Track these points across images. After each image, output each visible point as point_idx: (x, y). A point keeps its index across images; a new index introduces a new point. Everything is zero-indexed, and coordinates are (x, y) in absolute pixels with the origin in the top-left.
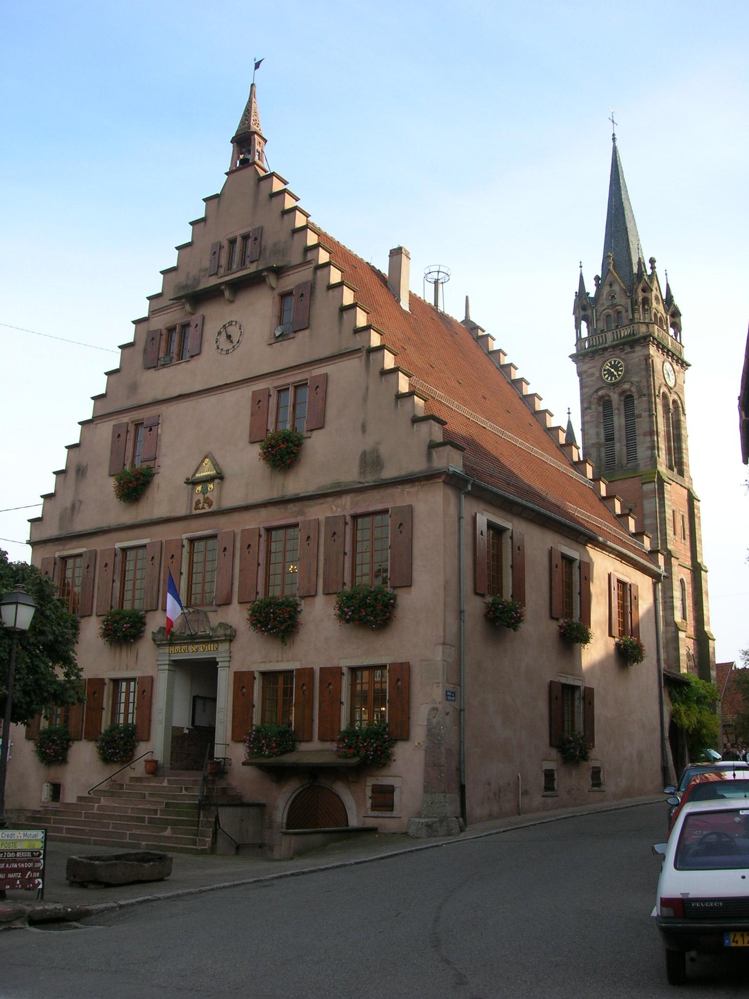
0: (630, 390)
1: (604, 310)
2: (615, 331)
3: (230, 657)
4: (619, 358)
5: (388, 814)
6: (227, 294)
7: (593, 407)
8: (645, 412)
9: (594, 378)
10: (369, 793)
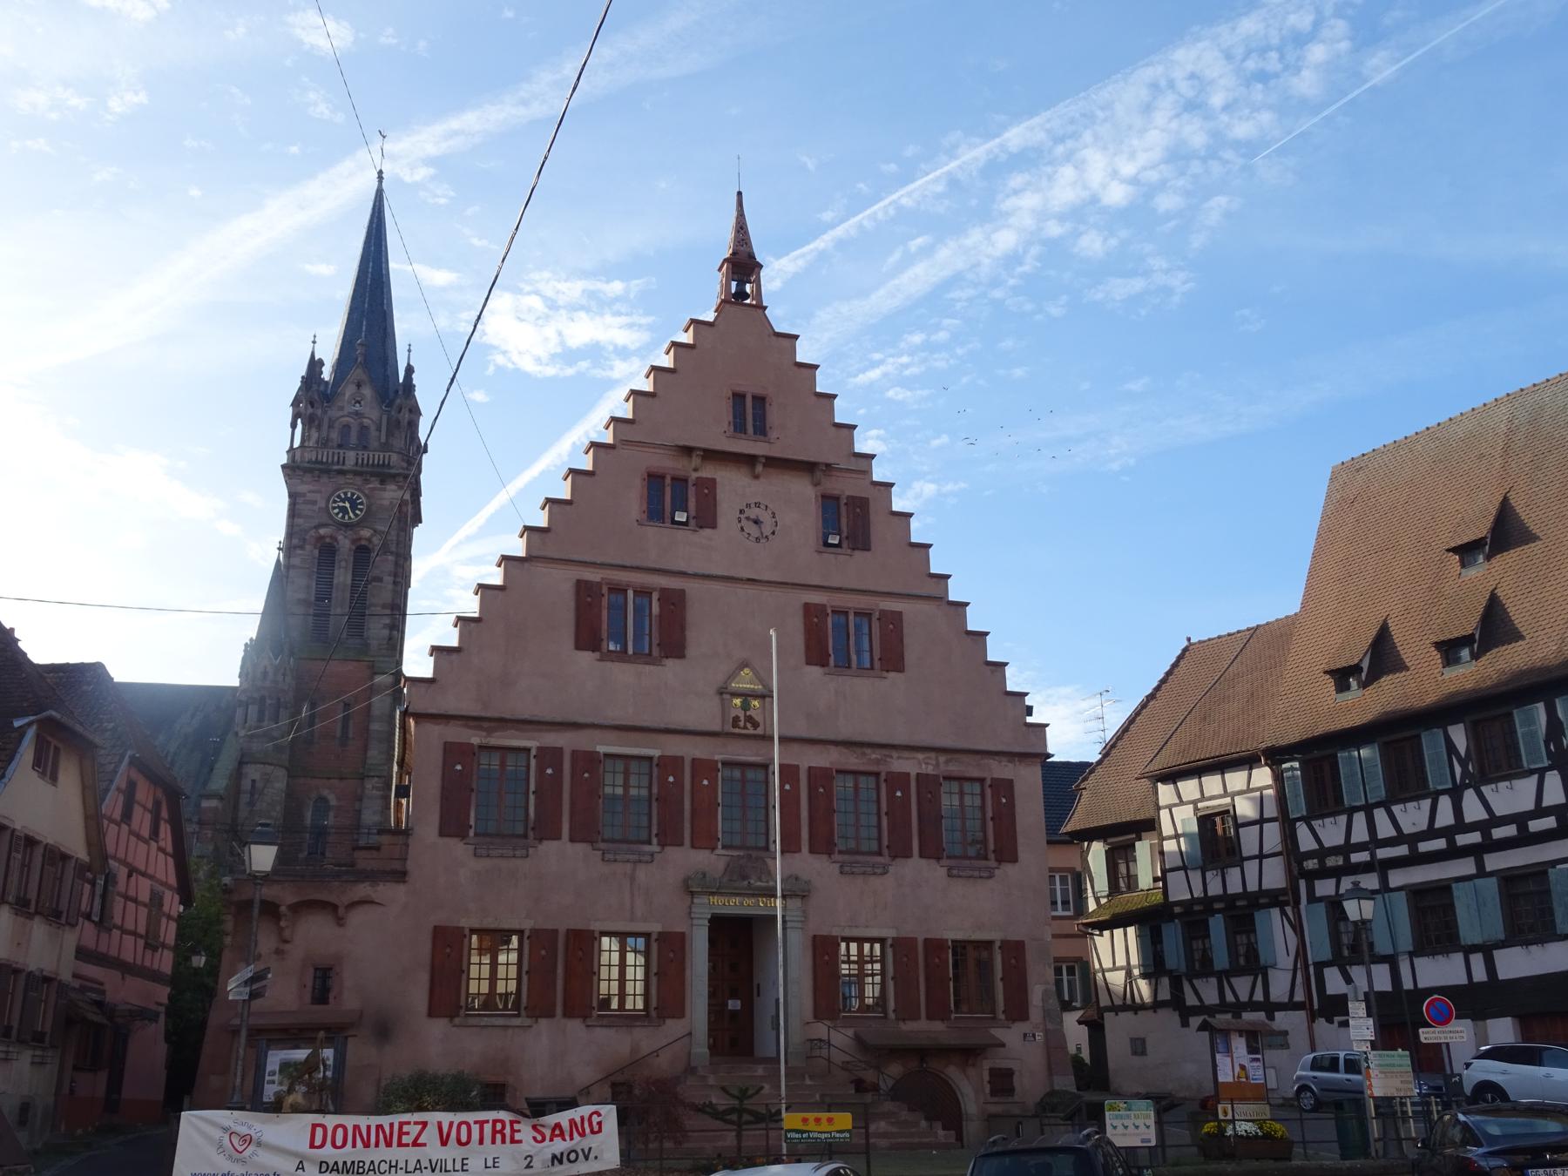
1: (343, 416)
2: (360, 453)
3: (805, 917)
4: (359, 490)
5: (1010, 1099)
6: (759, 468)
7: (308, 547)
8: (390, 575)
10: (986, 1077)
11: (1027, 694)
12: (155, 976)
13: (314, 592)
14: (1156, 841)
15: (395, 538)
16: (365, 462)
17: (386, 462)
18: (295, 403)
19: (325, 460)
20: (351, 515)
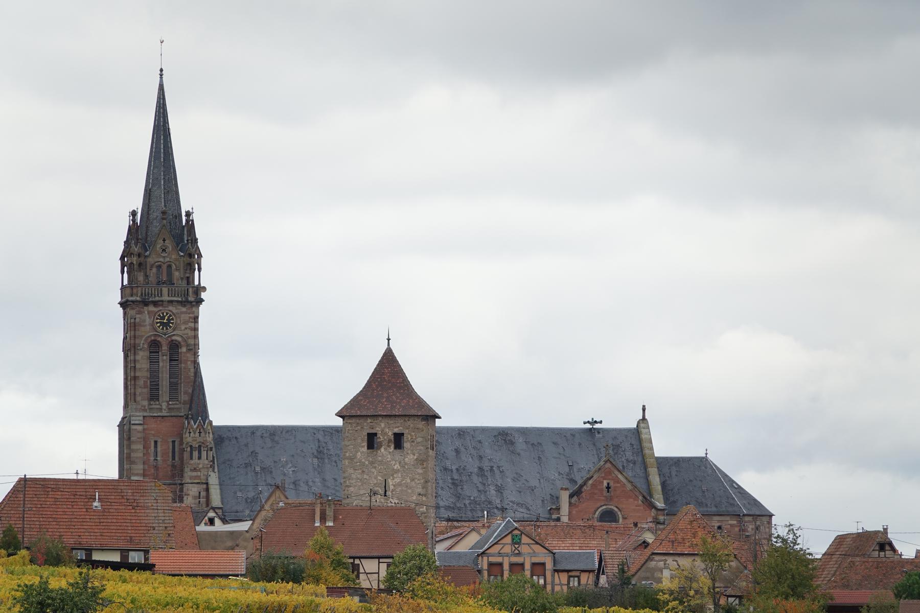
11: (439, 418)
14: (84, 558)
18: (122, 258)
20: (159, 321)
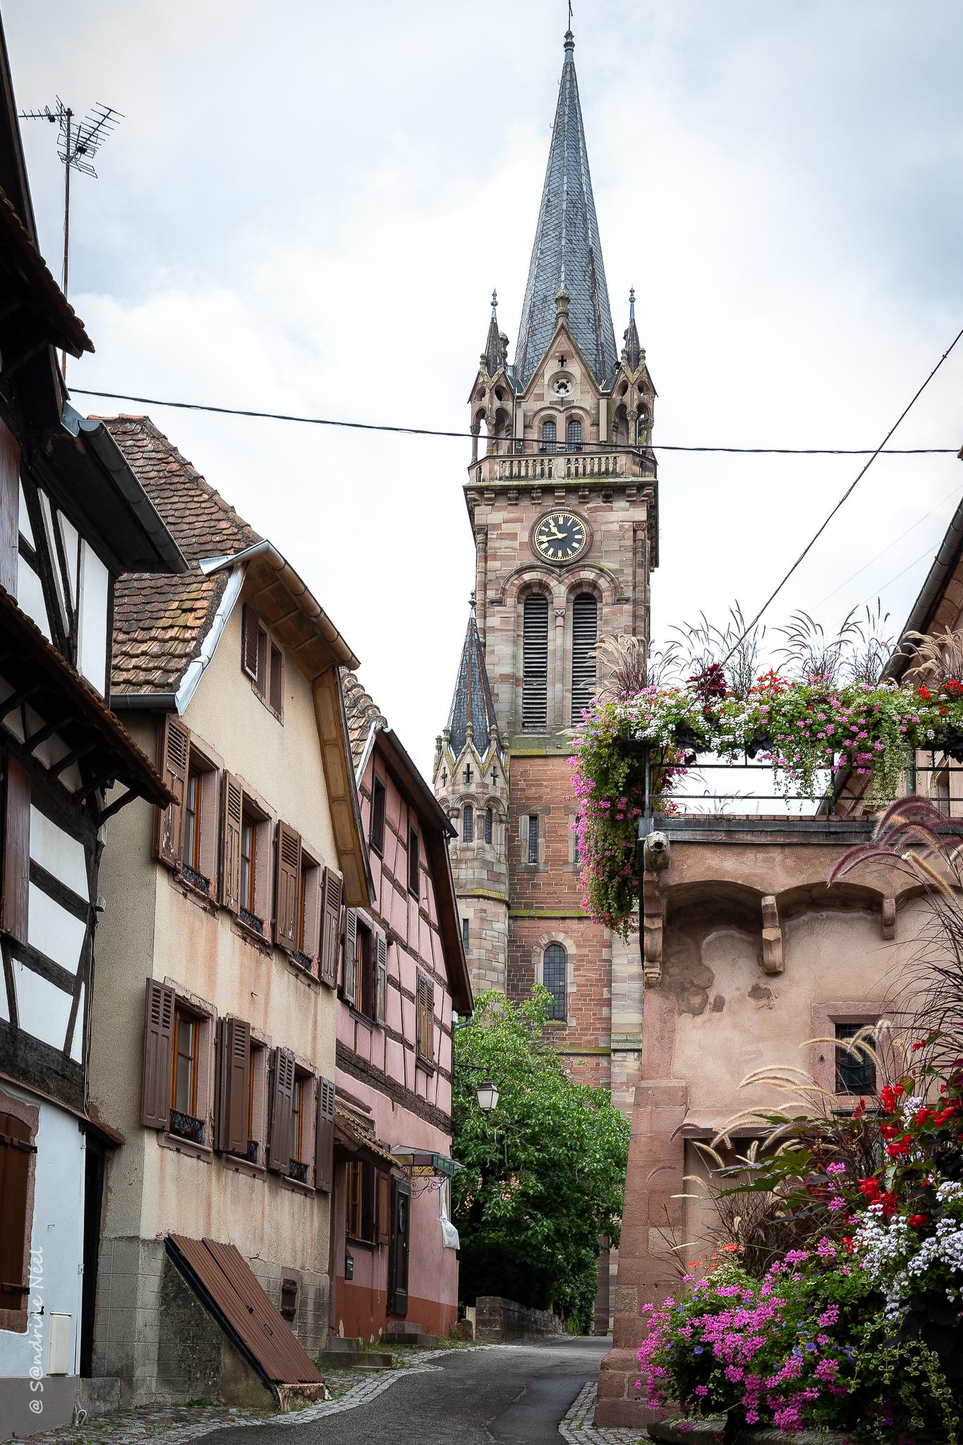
0: (594, 585)
2: (573, 458)
7: (510, 601)
9: (516, 544)
12: (428, 1112)
13: (521, 665)
15: (630, 578)
16: (581, 470)
17: (611, 469)
19: (523, 473)
